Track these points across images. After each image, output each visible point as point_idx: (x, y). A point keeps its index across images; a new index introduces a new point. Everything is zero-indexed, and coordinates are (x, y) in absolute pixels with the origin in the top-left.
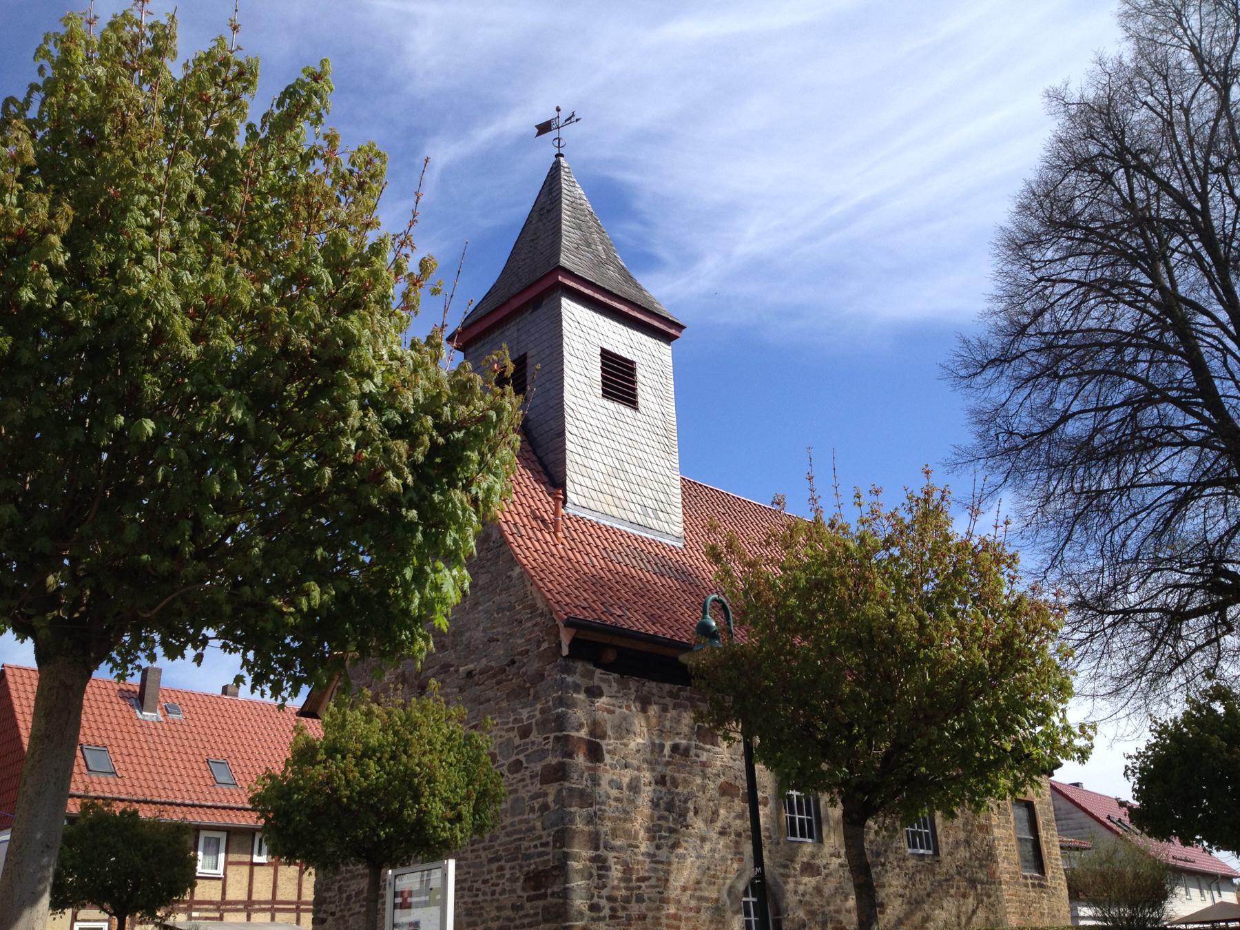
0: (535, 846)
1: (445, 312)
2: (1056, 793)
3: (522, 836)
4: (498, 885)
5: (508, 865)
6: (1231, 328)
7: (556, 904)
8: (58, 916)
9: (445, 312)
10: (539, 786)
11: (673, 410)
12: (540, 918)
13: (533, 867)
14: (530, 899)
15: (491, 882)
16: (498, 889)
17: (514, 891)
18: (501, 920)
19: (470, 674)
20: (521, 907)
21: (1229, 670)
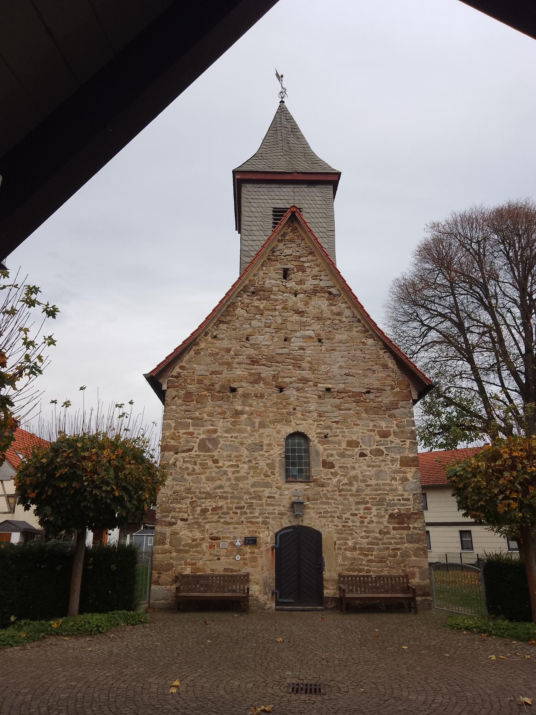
0: (399, 500)
1: (25, 386)
2: (303, 166)
3: (386, 492)
4: (366, 518)
5: (374, 508)
6: (523, 377)
7: (418, 534)
8: (524, 203)
9: (25, 386)
10: (399, 466)
11: (516, 384)
12: (405, 540)
13: (396, 511)
14: (394, 528)
15: (359, 516)
16: (367, 520)
17: (381, 523)
18: (370, 539)
19: (328, 390)
20: (388, 533)
21: (535, 444)
